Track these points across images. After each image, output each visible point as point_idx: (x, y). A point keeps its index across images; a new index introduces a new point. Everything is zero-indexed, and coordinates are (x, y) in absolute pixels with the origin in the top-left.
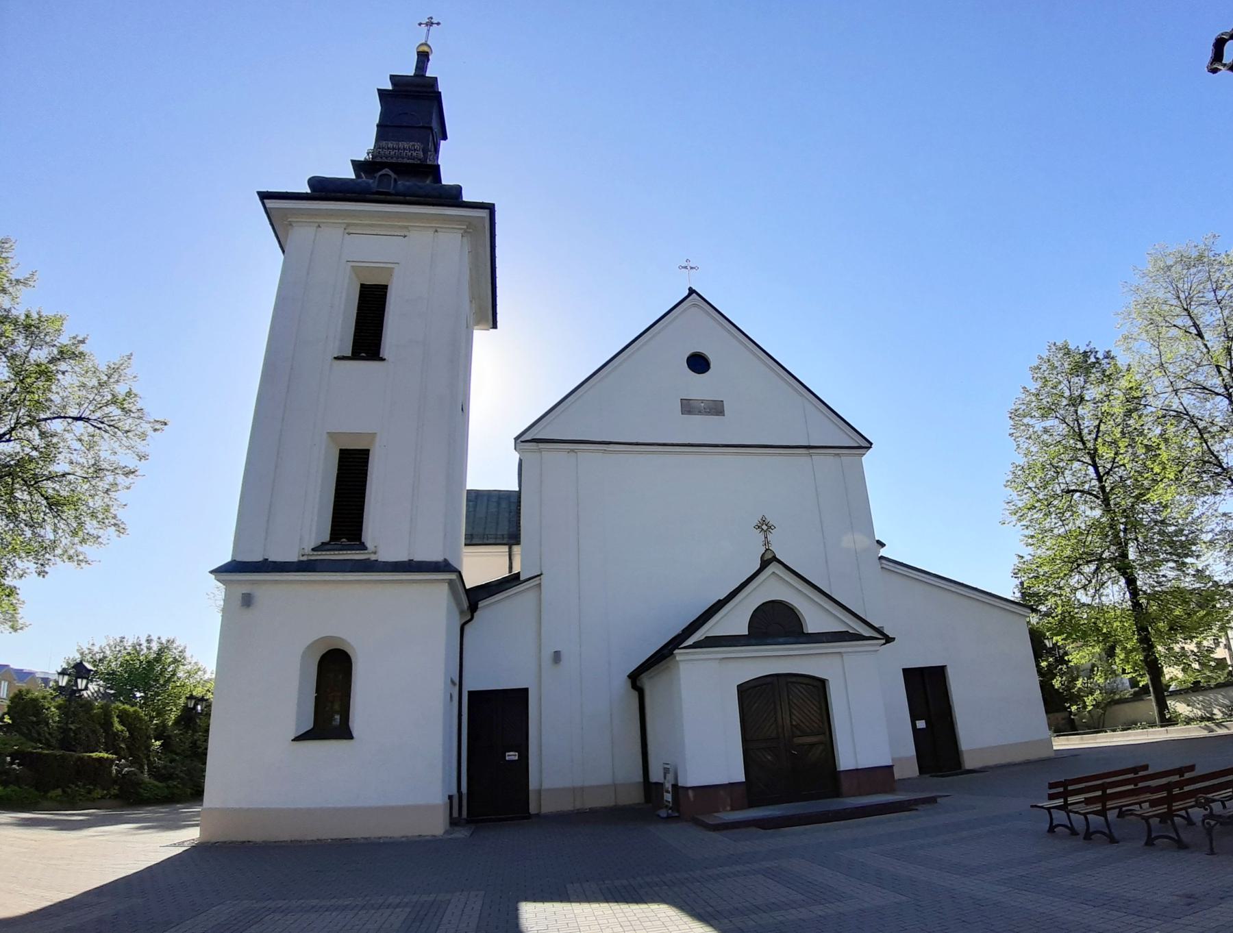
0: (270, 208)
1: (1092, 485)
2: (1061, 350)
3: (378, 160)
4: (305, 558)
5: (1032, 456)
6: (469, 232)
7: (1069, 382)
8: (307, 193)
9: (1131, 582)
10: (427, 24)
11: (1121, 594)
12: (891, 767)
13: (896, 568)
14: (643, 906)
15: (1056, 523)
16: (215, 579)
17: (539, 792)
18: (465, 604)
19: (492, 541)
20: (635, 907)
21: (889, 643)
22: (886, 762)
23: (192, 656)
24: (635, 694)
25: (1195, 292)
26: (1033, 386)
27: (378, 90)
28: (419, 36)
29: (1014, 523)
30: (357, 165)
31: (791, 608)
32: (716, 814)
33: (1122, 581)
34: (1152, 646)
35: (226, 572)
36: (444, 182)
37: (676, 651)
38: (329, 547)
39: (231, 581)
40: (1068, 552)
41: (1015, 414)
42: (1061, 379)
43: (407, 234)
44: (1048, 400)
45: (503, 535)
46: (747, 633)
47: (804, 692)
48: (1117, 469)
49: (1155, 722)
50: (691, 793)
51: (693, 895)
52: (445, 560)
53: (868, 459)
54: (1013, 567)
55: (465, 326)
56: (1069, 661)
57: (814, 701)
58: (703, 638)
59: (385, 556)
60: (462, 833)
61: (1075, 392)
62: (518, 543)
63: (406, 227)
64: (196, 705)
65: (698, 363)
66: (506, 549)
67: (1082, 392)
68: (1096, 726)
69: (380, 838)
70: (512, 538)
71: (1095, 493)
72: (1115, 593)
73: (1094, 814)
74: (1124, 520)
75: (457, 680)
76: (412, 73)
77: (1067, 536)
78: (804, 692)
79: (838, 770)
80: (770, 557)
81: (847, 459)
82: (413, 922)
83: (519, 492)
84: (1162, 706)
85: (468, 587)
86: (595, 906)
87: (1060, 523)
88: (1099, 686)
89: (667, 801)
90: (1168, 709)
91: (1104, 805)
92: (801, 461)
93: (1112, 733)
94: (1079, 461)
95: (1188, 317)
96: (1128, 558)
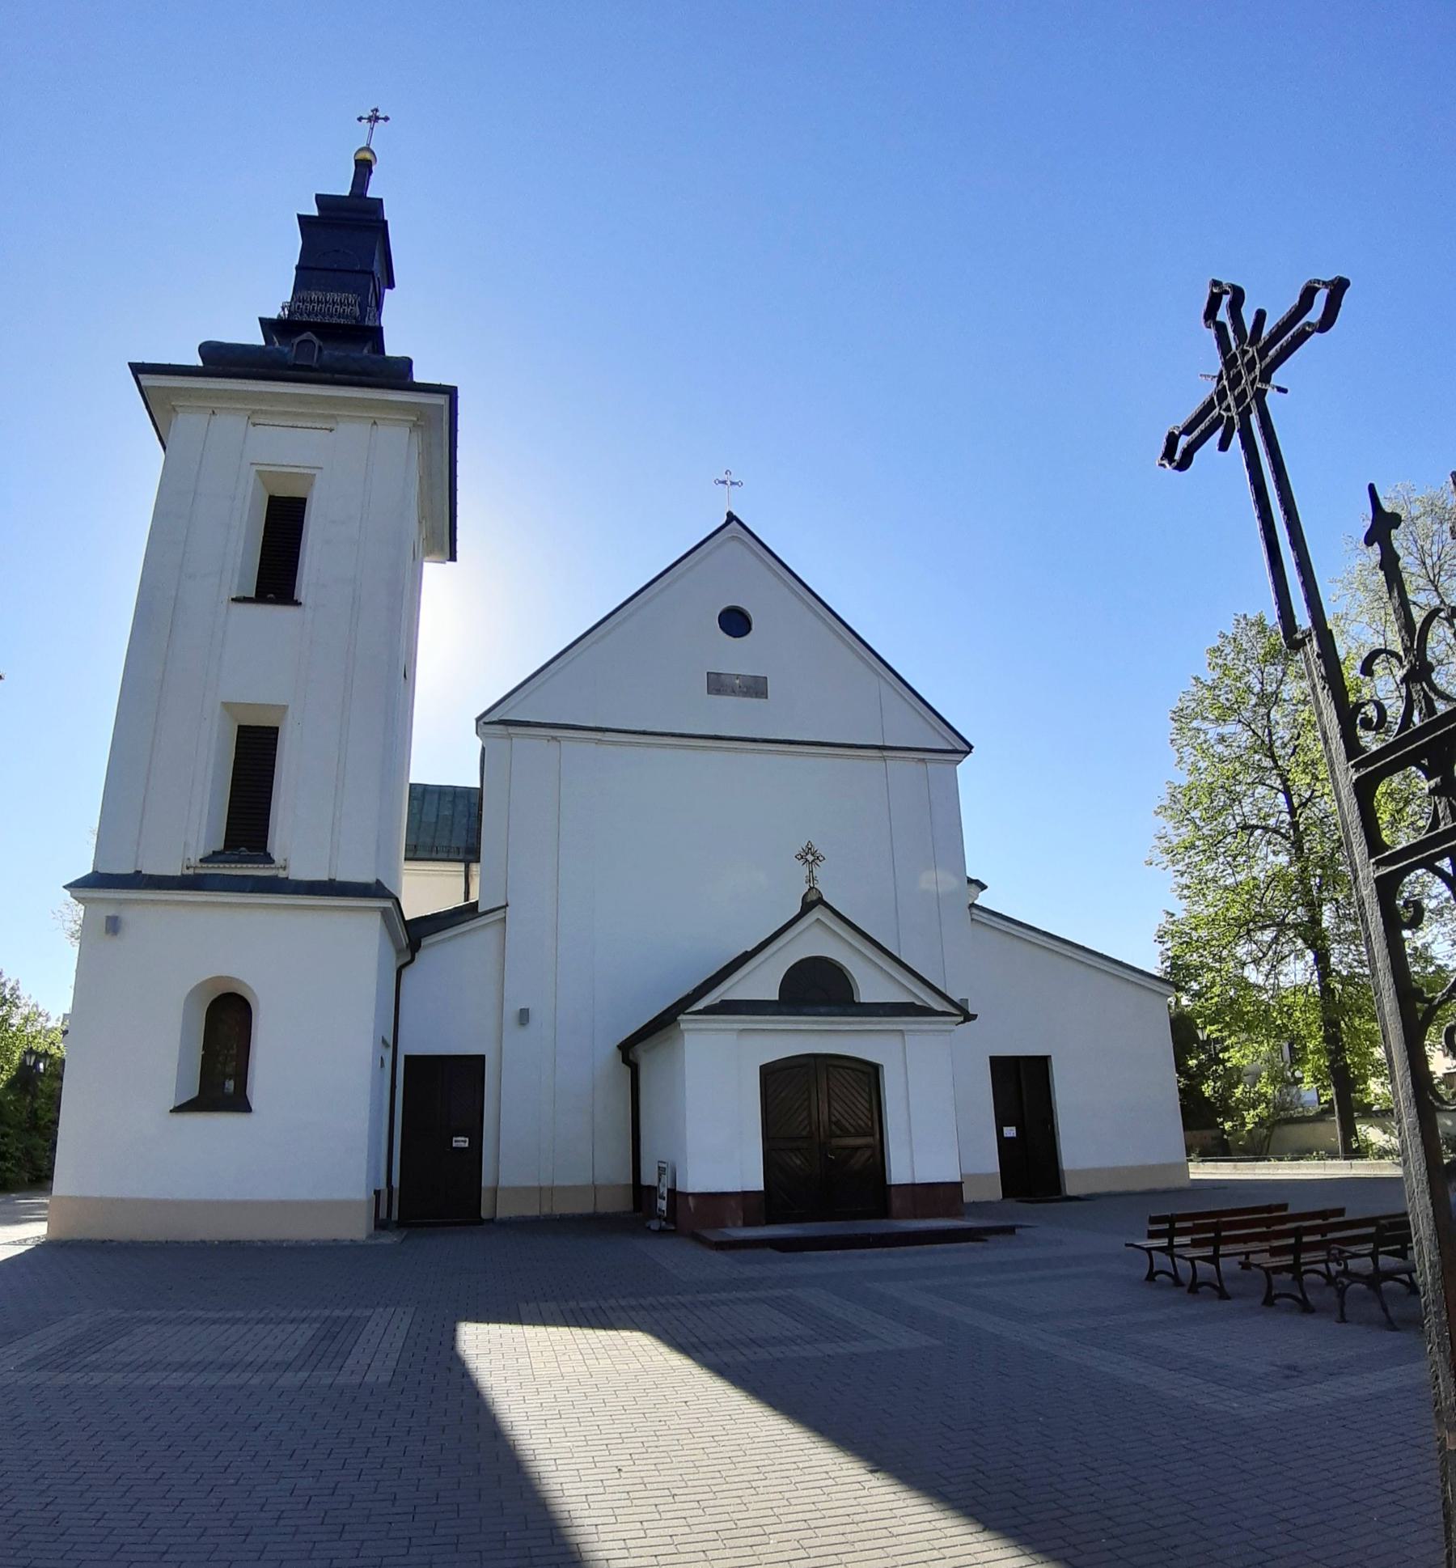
0: (146, 388)
1: (1280, 819)
2: (1253, 625)
3: (297, 317)
4: (191, 872)
5: (1200, 774)
6: (422, 426)
7: (1262, 673)
8: (197, 367)
9: (1322, 959)
10: (369, 119)
12: (958, 1186)
13: (991, 920)
15: (1224, 871)
16: (72, 896)
17: (495, 1190)
18: (404, 940)
19: (444, 856)
20: (601, 1333)
21: (969, 1021)
23: (30, 997)
24: (626, 1071)
25: (1448, 558)
26: (1209, 676)
27: (300, 217)
28: (359, 136)
29: (1164, 865)
30: (265, 323)
31: (839, 968)
32: (723, 1230)
33: (1310, 956)
34: (1341, 1049)
36: (388, 353)
37: (681, 1017)
38: (221, 858)
39: (93, 900)
40: (1235, 912)
41: (1179, 715)
42: (1251, 667)
44: (1229, 696)
45: (458, 848)
46: (777, 998)
47: (851, 1081)
48: (1317, 800)
49: (1338, 1153)
51: (676, 1322)
53: (965, 768)
56: (1228, 1060)
58: (718, 1001)
59: (300, 871)
60: (389, 1239)
61: (1268, 687)
62: (478, 861)
63: (333, 417)
64: (36, 1063)
65: (735, 622)
66: (461, 867)
67: (1278, 687)
68: (1257, 1151)
69: (283, 1241)
70: (469, 854)
71: (1283, 831)
72: (1298, 971)
74: (1319, 871)
75: (391, 1042)
76: (347, 193)
77: (1234, 889)
79: (888, 1183)
80: (815, 898)
81: (935, 768)
82: (322, 1340)
84: (1349, 1131)
85: (407, 918)
86: (551, 1329)
87: (1230, 871)
89: (660, 1210)
90: (1356, 1136)
92: (870, 767)
93: (1277, 1162)
94: (1264, 784)
95: (1435, 593)
96: (1320, 925)
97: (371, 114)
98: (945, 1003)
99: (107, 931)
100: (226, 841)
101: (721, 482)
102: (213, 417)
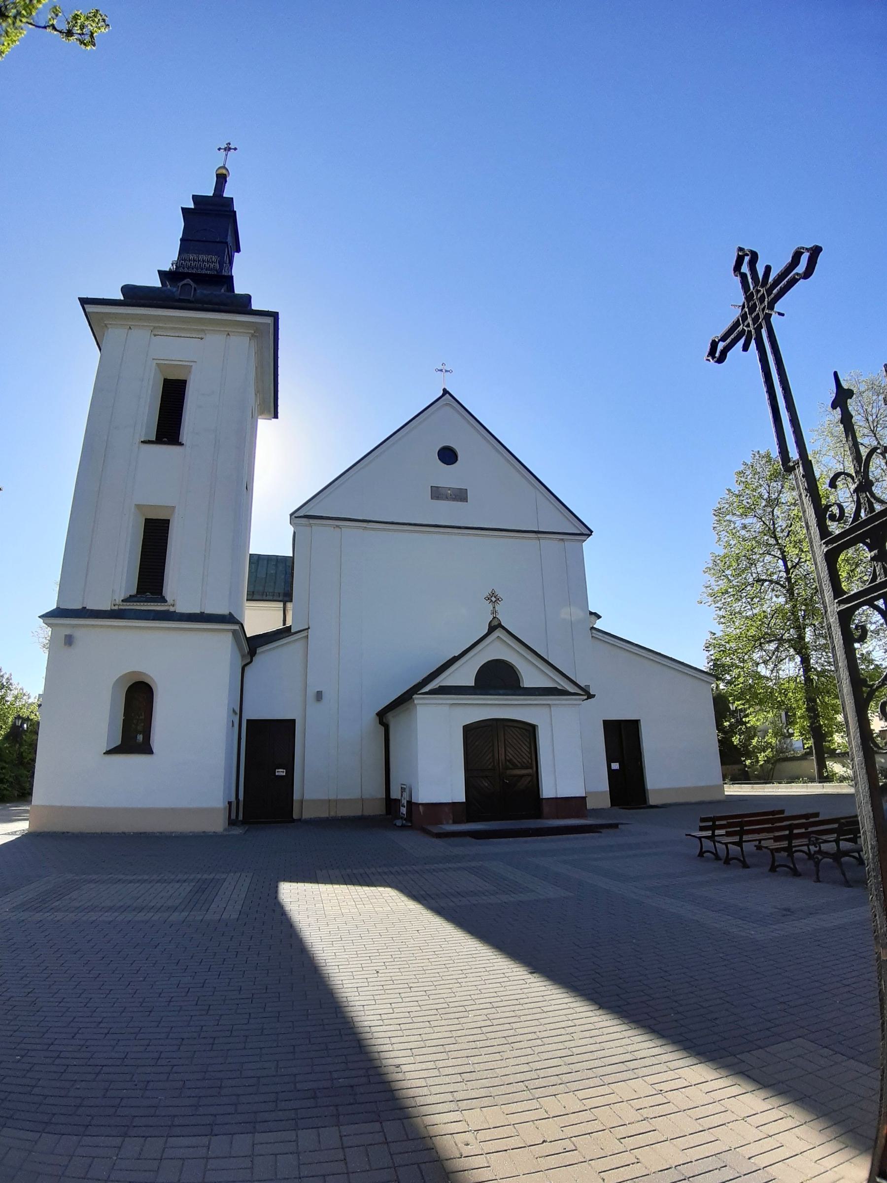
1: (780, 575)
2: (763, 457)
3: (181, 270)
4: (116, 608)
5: (731, 548)
7: (769, 486)
8: (120, 300)
9: (805, 661)
10: (225, 149)
11: (797, 670)
12: (584, 798)
13: (604, 637)
14: (372, 888)
16: (43, 622)
17: (302, 802)
19: (271, 598)
22: (579, 792)
24: (382, 729)
26: (737, 488)
27: (183, 209)
29: (709, 604)
32: (440, 826)
33: (798, 659)
35: (52, 617)
37: (415, 696)
38: (135, 599)
39: (56, 625)
40: (752, 632)
41: (718, 512)
42: (762, 483)
43: (203, 336)
44: (749, 501)
45: (279, 594)
46: (473, 685)
47: (519, 735)
48: (803, 564)
50: (421, 808)
52: (230, 614)
53: (588, 545)
54: (705, 642)
55: (251, 416)
56: (748, 722)
57: (525, 742)
58: (437, 687)
59: (182, 607)
60: (237, 831)
61: (772, 495)
62: (291, 601)
63: (203, 330)
65: (448, 455)
66: (281, 605)
68: (766, 778)
70: (286, 597)
71: (782, 583)
72: (791, 668)
73: (733, 844)
74: (803, 607)
77: (751, 618)
78: (519, 735)
79: (541, 797)
80: (496, 624)
81: (570, 544)
83: (293, 558)
84: (822, 765)
85: (248, 636)
87: (749, 607)
88: (771, 745)
90: (826, 769)
91: (741, 838)
92: (530, 544)
93: (778, 785)
94: (770, 554)
96: (804, 640)
97: (226, 146)
98: (576, 688)
99: (65, 644)
100: (138, 589)
101: (439, 370)
102: (130, 331)
